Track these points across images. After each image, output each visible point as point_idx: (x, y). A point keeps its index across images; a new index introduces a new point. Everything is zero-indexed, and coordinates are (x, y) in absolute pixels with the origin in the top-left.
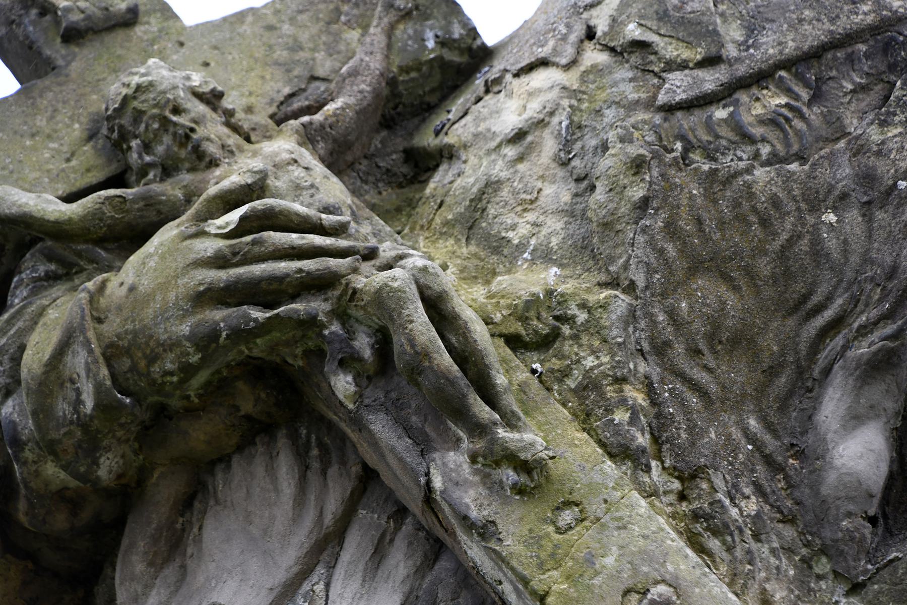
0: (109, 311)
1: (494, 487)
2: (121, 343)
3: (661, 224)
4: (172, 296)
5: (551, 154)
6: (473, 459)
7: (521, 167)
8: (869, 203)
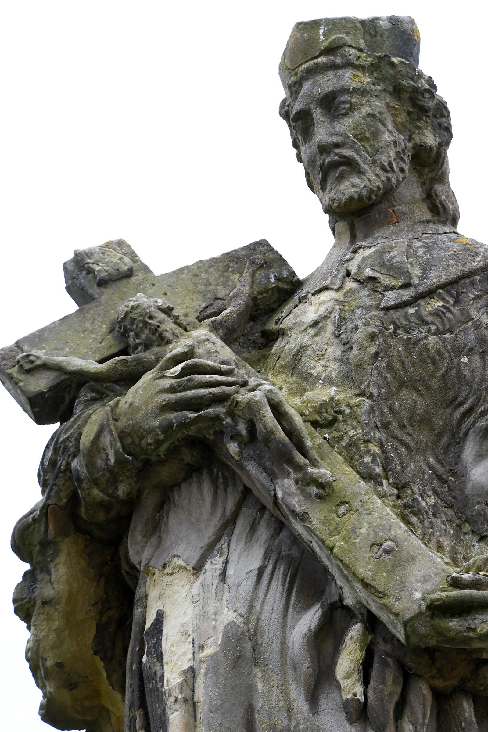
0: (120, 415)
1: (307, 496)
2: (126, 430)
4: (150, 407)
5: (331, 332)
7: (317, 339)
8: (483, 352)
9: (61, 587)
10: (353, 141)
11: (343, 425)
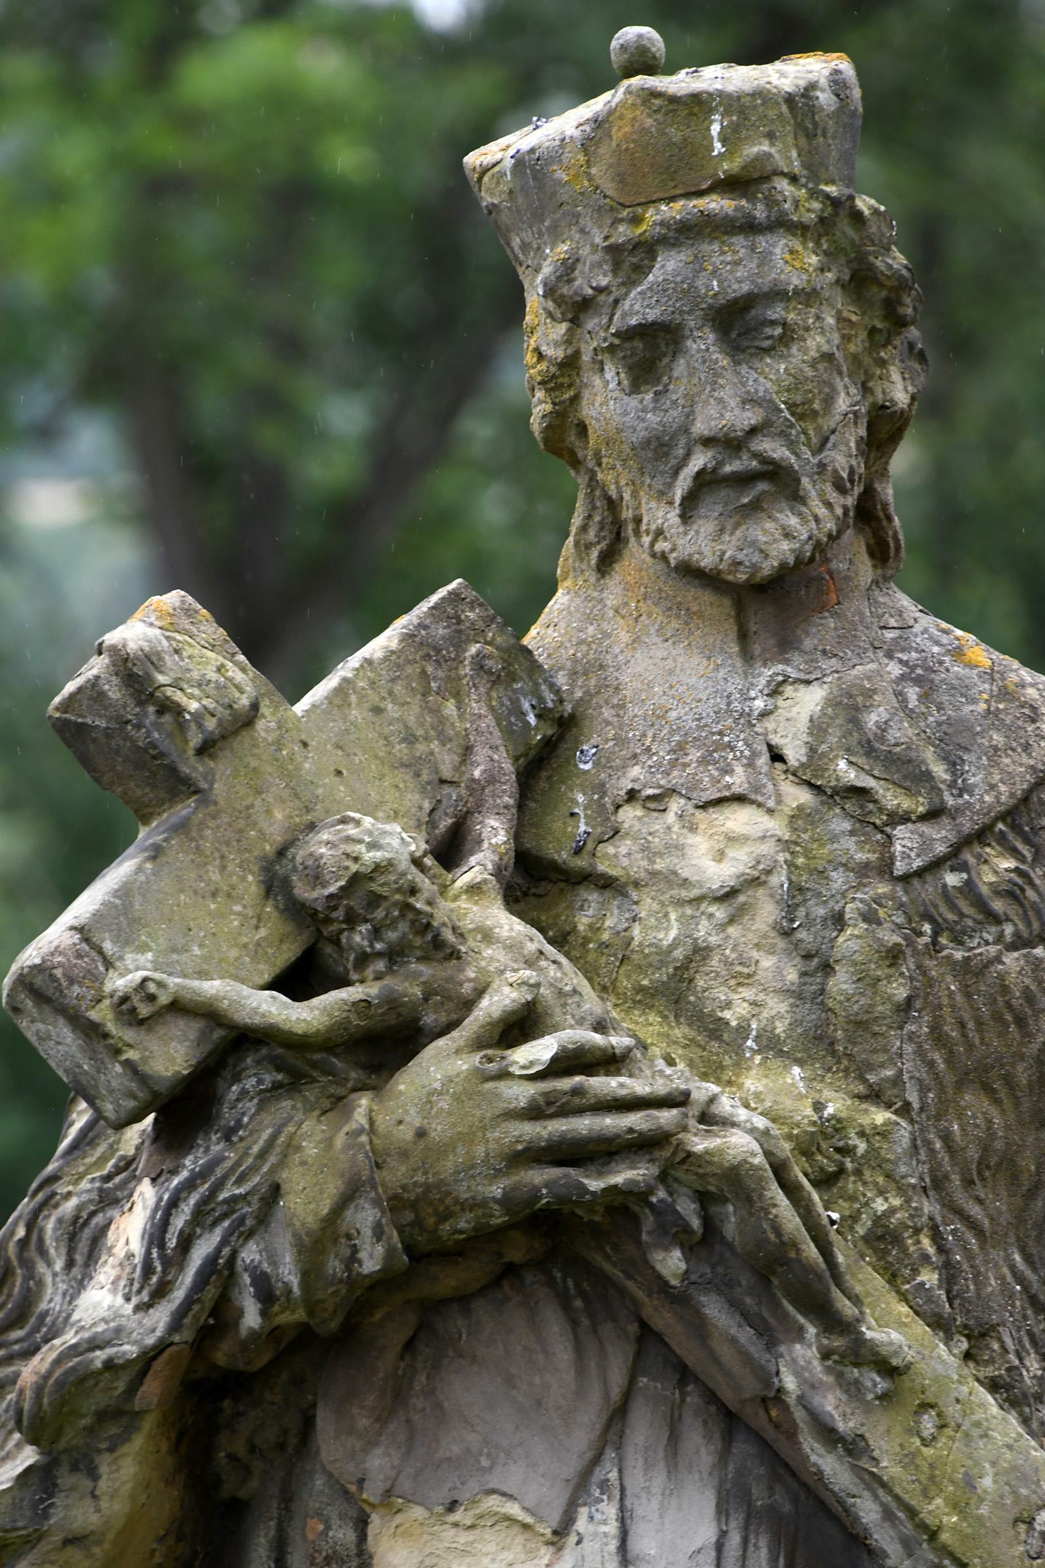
0: (388, 1155)
1: (853, 1390)
2: (406, 1195)
3: (926, 1029)
4: (480, 1151)
5: (771, 920)
6: (825, 1355)
7: (732, 930)
9: (117, 1507)
10: (787, 419)
11: (854, 1182)
